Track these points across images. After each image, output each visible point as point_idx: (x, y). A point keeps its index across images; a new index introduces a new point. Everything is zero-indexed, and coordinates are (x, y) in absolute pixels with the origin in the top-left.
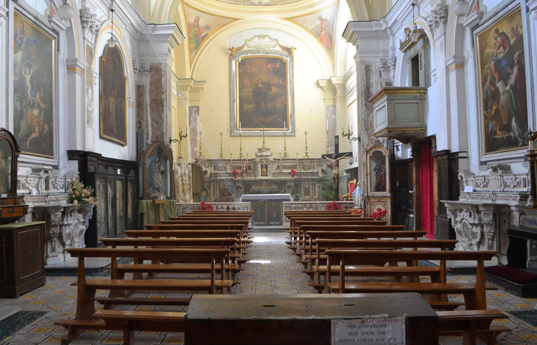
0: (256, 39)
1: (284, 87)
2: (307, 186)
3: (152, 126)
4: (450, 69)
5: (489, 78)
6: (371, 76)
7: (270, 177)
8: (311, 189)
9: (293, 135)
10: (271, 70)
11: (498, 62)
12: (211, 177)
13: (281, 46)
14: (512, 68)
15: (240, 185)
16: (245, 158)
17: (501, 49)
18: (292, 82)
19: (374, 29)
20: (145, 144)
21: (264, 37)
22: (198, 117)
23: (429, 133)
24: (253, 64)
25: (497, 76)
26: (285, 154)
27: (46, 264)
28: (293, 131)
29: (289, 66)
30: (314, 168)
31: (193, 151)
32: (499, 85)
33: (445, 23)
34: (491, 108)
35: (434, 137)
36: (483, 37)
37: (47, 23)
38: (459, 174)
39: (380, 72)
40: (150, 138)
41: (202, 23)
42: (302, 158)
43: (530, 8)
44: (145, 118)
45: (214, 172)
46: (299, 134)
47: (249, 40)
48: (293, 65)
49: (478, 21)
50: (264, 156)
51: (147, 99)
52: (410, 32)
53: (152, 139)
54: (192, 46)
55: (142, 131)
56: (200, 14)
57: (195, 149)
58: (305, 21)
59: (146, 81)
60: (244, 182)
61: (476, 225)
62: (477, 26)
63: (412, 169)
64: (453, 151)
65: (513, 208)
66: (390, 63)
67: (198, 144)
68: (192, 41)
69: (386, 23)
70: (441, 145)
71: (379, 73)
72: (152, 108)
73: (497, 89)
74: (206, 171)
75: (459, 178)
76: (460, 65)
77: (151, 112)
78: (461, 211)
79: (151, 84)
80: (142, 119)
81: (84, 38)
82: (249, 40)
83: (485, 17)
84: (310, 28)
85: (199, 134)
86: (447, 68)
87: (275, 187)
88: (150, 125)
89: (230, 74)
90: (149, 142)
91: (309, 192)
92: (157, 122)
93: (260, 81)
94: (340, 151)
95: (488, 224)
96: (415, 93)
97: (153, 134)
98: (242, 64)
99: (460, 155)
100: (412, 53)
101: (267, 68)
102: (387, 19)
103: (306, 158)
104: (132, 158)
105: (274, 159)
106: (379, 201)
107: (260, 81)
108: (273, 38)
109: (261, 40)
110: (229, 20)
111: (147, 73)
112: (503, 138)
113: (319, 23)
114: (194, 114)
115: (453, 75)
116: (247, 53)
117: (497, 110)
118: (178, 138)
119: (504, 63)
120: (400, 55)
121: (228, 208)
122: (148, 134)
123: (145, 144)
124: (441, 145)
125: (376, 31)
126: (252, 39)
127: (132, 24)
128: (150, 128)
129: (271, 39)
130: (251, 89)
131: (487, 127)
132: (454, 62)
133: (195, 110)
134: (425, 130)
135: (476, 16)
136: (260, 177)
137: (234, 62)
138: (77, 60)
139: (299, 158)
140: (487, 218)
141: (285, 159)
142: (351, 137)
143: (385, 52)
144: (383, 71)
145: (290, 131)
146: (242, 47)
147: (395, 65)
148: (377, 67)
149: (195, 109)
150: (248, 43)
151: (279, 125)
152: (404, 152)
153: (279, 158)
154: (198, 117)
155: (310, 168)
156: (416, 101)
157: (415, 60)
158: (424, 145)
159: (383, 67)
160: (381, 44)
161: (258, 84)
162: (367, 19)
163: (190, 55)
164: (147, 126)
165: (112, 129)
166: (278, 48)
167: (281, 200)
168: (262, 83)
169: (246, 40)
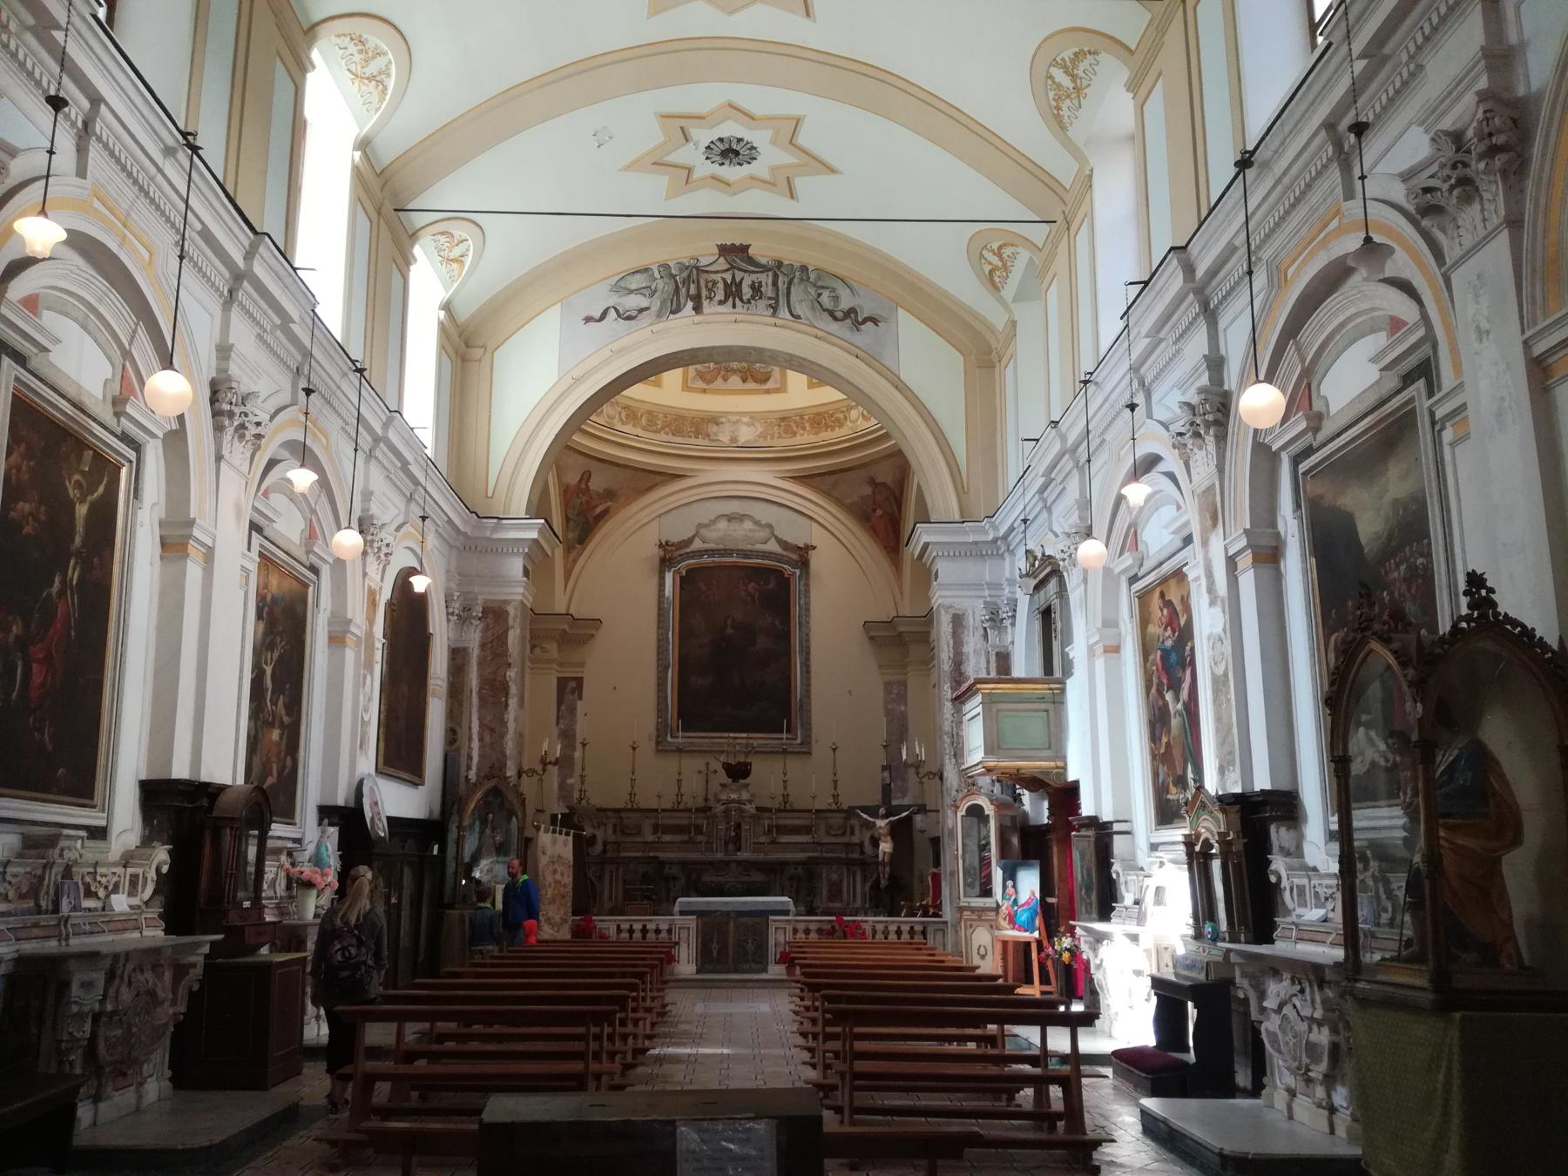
0: (722, 524)
1: (786, 636)
2: (835, 877)
3: (481, 740)
4: (1240, 566)
5: (1155, 680)
6: (966, 639)
7: (744, 855)
8: (845, 885)
9: (805, 750)
11: (1166, 654)
12: (604, 851)
13: (779, 541)
15: (675, 871)
16: (689, 806)
17: (1169, 632)
18: (805, 625)
19: (971, 539)
20: (462, 780)
21: (741, 518)
22: (579, 703)
23: (1071, 777)
28: (807, 741)
29: (796, 586)
30: (852, 833)
31: (562, 786)
36: (1143, 597)
37: (303, 559)
40: (474, 768)
41: (596, 484)
42: (824, 807)
43: (1439, 414)
44: (465, 724)
45: (612, 838)
46: (820, 749)
47: (706, 526)
48: (807, 585)
49: (1135, 570)
50: (734, 801)
51: (473, 679)
52: (1035, 558)
53: (479, 769)
54: (571, 535)
55: (458, 750)
56: (593, 465)
57: (569, 781)
59: (473, 639)
60: (684, 864)
62: (1309, 451)
63: (1050, 848)
64: (1105, 819)
66: (1005, 612)
67: (577, 771)
68: (572, 524)
69: (996, 528)
72: (482, 699)
73: (1166, 705)
74: (594, 836)
76: (1268, 555)
77: (481, 708)
79: (483, 646)
80: (459, 724)
81: (365, 574)
82: (706, 526)
83: (1328, 429)
84: (848, 501)
85: (579, 746)
86: (1231, 562)
87: (757, 877)
88: (475, 737)
89: (660, 602)
90: (472, 775)
91: (840, 891)
92: (492, 730)
97: (481, 756)
98: (687, 581)
99: (1116, 827)
102: (997, 519)
103: (834, 807)
104: (431, 812)
105: (758, 809)
106: (980, 919)
109: (735, 526)
111: (475, 622)
112: (97, 1099)
113: (868, 490)
114: (569, 697)
115: (1247, 581)
116: (701, 556)
117: (1168, 744)
118: (539, 768)
119: (1173, 657)
121: (644, 931)
122: (470, 758)
123: (462, 780)
125: (976, 543)
126: (714, 522)
127: (450, 521)
128: (476, 745)
129: (757, 523)
131: (1155, 774)
132: (1249, 546)
133: (570, 689)
134: (1065, 768)
135: (1304, 425)
137: (669, 577)
138: (350, 622)
139: (818, 807)
141: (785, 811)
143: (996, 586)
144: (993, 628)
145: (799, 741)
146: (690, 541)
147: (1014, 617)
148: (978, 619)
149: (573, 684)
150: (703, 531)
151: (770, 725)
152: (1037, 809)
153: (769, 805)
154: (579, 703)
155: (844, 834)
156: (1043, 706)
158: (1066, 797)
159: (991, 619)
160: (986, 571)
162: (957, 518)
163: (566, 557)
164: (470, 739)
165: (400, 752)
166: (773, 546)
167: (764, 914)
169: (700, 526)
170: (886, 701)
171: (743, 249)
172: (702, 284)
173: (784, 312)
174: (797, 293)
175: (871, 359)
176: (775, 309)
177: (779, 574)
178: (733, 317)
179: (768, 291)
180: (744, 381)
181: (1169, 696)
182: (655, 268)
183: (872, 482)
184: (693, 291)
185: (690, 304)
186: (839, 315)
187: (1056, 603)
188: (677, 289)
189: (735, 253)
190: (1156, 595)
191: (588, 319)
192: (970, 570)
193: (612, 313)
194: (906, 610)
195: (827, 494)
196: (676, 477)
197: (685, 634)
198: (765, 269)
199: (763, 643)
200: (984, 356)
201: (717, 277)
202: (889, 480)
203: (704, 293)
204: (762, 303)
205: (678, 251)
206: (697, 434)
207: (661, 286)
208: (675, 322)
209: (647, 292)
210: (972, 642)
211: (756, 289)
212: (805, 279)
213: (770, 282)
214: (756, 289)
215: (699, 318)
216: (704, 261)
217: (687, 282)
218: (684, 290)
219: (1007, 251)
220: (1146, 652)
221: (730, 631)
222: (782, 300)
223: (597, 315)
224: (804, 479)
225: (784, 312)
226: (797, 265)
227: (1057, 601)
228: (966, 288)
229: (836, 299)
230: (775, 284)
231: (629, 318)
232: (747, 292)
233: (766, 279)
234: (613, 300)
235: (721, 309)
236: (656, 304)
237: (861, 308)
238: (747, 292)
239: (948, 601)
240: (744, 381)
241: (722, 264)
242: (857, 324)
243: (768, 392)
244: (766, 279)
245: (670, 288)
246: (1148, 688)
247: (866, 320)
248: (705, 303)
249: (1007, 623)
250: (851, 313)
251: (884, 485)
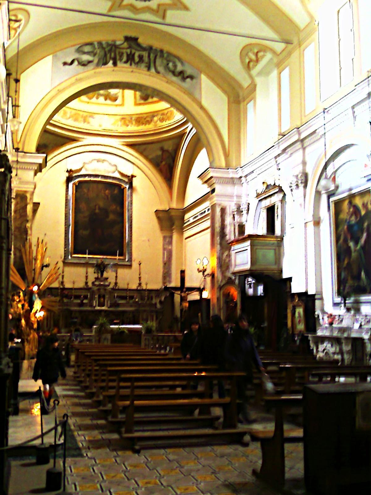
10: (109, 196)
11: (350, 227)
14: (362, 234)
23: (285, 276)
24: (91, 189)
25: (349, 237)
26: (116, 284)
27: (321, 330)
28: (130, 260)
29: (127, 192)
32: (351, 244)
33: (305, 186)
34: (344, 260)
35: (290, 279)
38: (316, 313)
39: (234, 215)
46: (135, 265)
58: (145, 150)
61: (338, 354)
65: (366, 341)
66: (244, 207)
70: (296, 288)
71: (232, 216)
75: (316, 316)
76: (317, 223)
78: (322, 342)
84: (150, 157)
93: (97, 207)
94: (188, 284)
95: (348, 352)
96: (271, 240)
98: (78, 187)
100: (267, 203)
101: (105, 194)
107: (97, 207)
108: (113, 164)
110: (65, 140)
113: (159, 153)
117: (348, 264)
119: (356, 228)
120: (254, 202)
124: (296, 288)
125: (232, 178)
126: (91, 162)
130: (87, 214)
134: (281, 271)
136: (98, 308)
137: (71, 185)
140: (346, 348)
142: (206, 273)
143: (239, 197)
145: (127, 260)
146: (80, 170)
157: (271, 211)
161: (95, 209)
166: (118, 175)
168: (99, 208)
169: (84, 163)
170: (164, 245)
171: (136, 39)
172: (117, 53)
173: (153, 70)
174: (158, 61)
175: (189, 93)
176: (149, 69)
177: (120, 186)
178: (130, 70)
179: (146, 59)
180: (106, 99)
181: (351, 244)
182: (96, 43)
183: (162, 149)
184: (113, 55)
185: (111, 62)
186: (177, 73)
187: (278, 205)
188: (105, 55)
189: (131, 40)
190: (346, 202)
191: (65, 64)
192: (229, 189)
193: (76, 63)
194: (174, 205)
195: (141, 153)
196: (74, 140)
197: (77, 210)
198: (144, 49)
199: (112, 217)
200: (238, 97)
201: (124, 51)
202: (170, 149)
203: (118, 57)
204: (143, 65)
205: (106, 37)
206: (85, 121)
207: (98, 52)
208: (103, 69)
209: (92, 54)
210: (228, 220)
211: (141, 58)
212: (162, 56)
213: (147, 55)
214: (141, 58)
215: (116, 68)
216: (118, 43)
217: (110, 51)
218: (108, 56)
219: (260, 54)
220: (337, 223)
221: (97, 211)
222: (152, 65)
223: (69, 61)
224: (131, 145)
225: (153, 70)
226: (158, 49)
227: (280, 204)
228: (234, 68)
229: (175, 66)
230: (149, 56)
231: (84, 65)
232: (137, 59)
233: (145, 54)
234: (76, 56)
235: (125, 65)
236: (96, 61)
237: (186, 72)
238: (137, 59)
239: (219, 202)
240: (106, 99)
241: (126, 45)
242: (184, 79)
243: (117, 105)
244: (145, 54)
245: (102, 53)
246: (337, 240)
247: (188, 77)
248: (118, 62)
249: (245, 212)
250: (181, 73)
251: (167, 151)
